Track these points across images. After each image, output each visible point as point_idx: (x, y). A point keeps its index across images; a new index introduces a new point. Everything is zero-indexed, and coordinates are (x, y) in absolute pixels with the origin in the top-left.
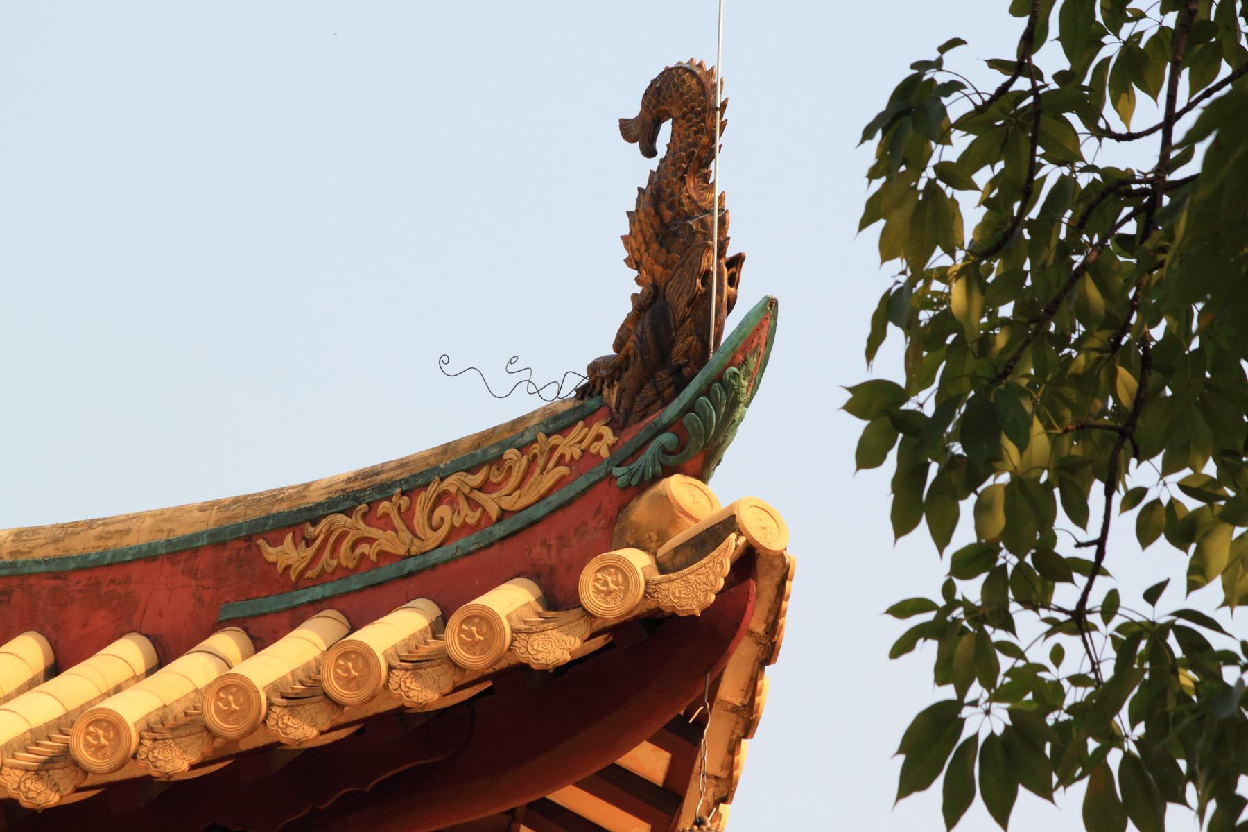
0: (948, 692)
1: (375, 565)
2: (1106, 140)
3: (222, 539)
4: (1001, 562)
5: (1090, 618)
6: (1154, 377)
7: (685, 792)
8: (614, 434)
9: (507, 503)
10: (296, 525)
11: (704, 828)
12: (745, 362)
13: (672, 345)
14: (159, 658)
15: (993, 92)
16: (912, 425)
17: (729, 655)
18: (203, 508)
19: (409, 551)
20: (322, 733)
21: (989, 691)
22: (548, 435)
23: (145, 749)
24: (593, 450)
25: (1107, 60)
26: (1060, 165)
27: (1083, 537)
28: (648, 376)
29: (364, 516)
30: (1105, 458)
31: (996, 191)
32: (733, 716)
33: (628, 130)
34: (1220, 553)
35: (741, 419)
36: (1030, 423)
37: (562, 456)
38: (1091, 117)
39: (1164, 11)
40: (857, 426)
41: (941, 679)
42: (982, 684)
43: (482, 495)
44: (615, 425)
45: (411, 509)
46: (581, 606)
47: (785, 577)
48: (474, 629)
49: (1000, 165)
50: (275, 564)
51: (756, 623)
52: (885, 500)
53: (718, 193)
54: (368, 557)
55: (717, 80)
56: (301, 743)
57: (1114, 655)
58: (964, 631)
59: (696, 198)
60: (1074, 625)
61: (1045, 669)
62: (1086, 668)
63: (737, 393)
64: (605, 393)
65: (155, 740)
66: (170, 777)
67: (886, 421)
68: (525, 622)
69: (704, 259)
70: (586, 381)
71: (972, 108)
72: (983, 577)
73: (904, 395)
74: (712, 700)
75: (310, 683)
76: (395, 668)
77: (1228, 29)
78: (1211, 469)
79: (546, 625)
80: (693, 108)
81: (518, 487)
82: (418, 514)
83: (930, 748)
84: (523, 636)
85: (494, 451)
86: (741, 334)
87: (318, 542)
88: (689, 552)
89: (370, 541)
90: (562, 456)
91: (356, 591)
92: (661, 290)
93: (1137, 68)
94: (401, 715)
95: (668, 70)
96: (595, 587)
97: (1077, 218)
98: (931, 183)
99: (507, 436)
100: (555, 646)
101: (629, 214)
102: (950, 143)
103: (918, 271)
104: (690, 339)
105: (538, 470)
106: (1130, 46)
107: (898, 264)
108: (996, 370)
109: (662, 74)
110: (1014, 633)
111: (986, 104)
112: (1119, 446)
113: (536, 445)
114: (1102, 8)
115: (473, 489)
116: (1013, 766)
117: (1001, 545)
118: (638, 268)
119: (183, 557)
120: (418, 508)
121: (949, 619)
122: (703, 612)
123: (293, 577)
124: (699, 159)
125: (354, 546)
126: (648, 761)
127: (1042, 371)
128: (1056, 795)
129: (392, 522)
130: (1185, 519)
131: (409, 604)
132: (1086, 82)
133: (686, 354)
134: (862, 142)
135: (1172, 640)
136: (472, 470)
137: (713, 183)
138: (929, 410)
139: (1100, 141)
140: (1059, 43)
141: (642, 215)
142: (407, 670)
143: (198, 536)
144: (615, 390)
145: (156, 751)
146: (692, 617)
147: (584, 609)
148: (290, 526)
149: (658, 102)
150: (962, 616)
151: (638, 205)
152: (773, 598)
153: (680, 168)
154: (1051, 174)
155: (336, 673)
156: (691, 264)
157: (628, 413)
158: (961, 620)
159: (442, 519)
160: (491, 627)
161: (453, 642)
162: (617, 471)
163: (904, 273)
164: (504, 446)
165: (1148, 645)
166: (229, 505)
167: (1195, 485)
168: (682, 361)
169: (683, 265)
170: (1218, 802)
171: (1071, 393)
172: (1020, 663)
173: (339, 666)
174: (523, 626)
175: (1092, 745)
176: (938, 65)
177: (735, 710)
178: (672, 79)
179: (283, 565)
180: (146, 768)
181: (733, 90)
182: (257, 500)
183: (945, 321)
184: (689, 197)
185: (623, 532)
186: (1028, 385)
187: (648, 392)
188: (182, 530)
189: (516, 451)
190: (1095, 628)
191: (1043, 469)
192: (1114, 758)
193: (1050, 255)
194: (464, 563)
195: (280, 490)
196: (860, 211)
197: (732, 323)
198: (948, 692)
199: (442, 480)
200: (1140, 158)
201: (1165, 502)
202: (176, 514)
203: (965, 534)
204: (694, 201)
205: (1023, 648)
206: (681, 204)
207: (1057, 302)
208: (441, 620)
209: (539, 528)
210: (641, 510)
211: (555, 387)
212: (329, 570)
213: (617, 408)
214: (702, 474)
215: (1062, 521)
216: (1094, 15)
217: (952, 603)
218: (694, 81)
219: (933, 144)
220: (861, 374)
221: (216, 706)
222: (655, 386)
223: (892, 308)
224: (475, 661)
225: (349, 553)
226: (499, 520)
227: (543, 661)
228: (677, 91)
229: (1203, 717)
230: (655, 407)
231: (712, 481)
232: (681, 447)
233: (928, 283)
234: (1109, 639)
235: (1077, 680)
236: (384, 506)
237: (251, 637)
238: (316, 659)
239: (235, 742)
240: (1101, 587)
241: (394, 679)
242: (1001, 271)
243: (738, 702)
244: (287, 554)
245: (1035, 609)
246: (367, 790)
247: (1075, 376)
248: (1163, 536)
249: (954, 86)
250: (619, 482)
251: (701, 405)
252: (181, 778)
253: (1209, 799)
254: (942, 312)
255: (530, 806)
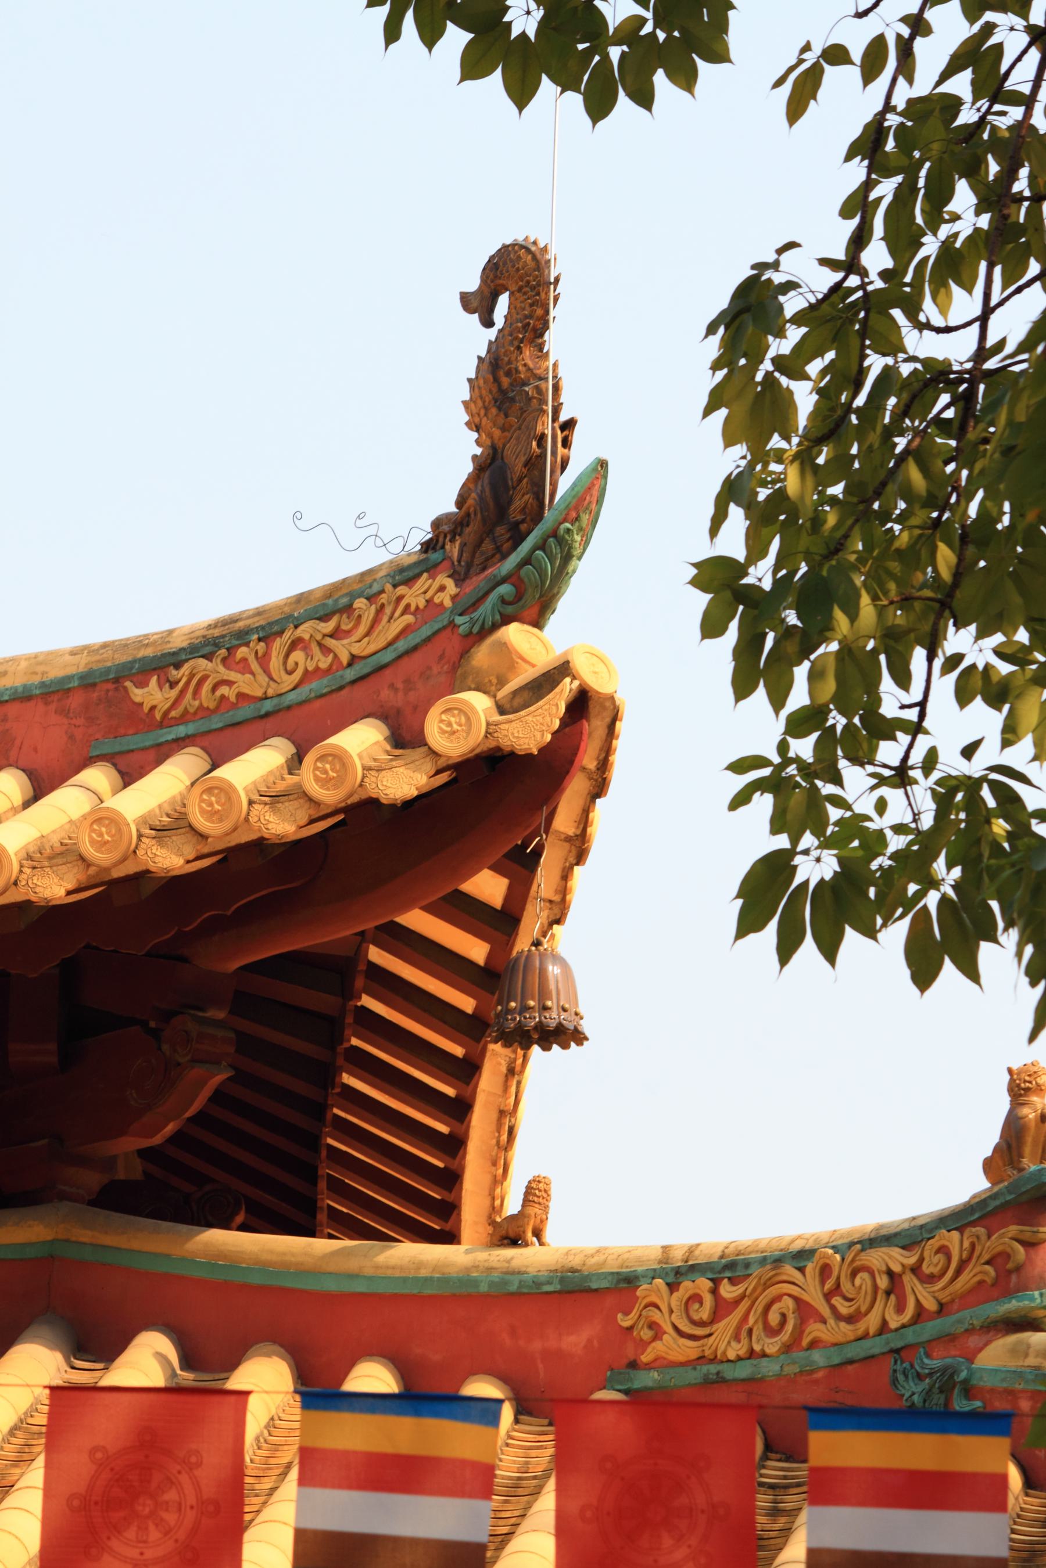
0: (783, 841)
1: (234, 706)
2: (926, 332)
3: (91, 681)
4: (831, 722)
5: (911, 773)
6: (971, 550)
7: (522, 915)
8: (456, 585)
9: (356, 649)
10: (161, 668)
11: (541, 948)
12: (577, 519)
13: (510, 502)
14: (34, 790)
15: (825, 291)
16: (750, 596)
17: (563, 791)
18: (73, 653)
19: (265, 693)
20: (188, 862)
21: (819, 839)
22: (395, 586)
23: (24, 876)
24: (437, 600)
25: (926, 258)
26: (884, 355)
27: (907, 699)
28: (488, 531)
29: (224, 660)
30: (926, 627)
31: (828, 378)
32: (567, 845)
33: (467, 302)
34: (1030, 714)
35: (574, 571)
36: (859, 596)
37: (408, 606)
38: (912, 311)
39: (978, 213)
40: (702, 600)
41: (775, 830)
42: (813, 833)
43: (333, 641)
44: (457, 577)
45: (267, 654)
46: (426, 744)
47: (615, 718)
48: (328, 766)
49: (831, 355)
50: (141, 704)
51: (588, 760)
52: (727, 666)
53: (552, 361)
54: (228, 699)
55: (550, 256)
56: (168, 871)
57: (934, 806)
58: (797, 785)
59: (531, 366)
60: (897, 780)
61: (869, 819)
62: (908, 818)
63: (570, 548)
64: (448, 547)
65: (34, 868)
66: (49, 901)
67: (728, 595)
68: (375, 760)
69: (540, 423)
70: (430, 536)
71: (806, 305)
72: (815, 736)
73: (741, 570)
74: (547, 832)
75: (176, 815)
76: (255, 802)
77: (1036, 230)
78: (1022, 636)
79: (394, 763)
80: (528, 282)
81: (367, 634)
82: (274, 659)
83: (765, 892)
84: (373, 773)
85: (344, 601)
86: (574, 493)
87: (181, 684)
88: (526, 695)
89: (229, 683)
90: (408, 606)
91: (215, 730)
92: (500, 451)
93: (953, 265)
94: (260, 845)
95: (505, 248)
96: (440, 728)
97: (902, 407)
98: (768, 375)
99: (356, 587)
100: (403, 782)
101: (469, 380)
102: (785, 337)
103: (759, 455)
104: (527, 497)
105: (385, 619)
106: (947, 246)
107: (740, 449)
108: (828, 548)
109: (500, 250)
110: (842, 787)
111: (820, 302)
112: (939, 615)
113: (383, 595)
114: (923, 211)
115: (325, 635)
116: (839, 911)
117: (832, 706)
118: (477, 431)
119: (56, 698)
120: (274, 653)
121: (783, 774)
122: (540, 750)
123: (158, 716)
124: (535, 330)
125: (214, 688)
126: (488, 886)
127: (869, 547)
128: (879, 936)
129: (249, 666)
130: (999, 683)
131: (267, 742)
132: (908, 279)
133: (523, 510)
134: (706, 337)
135: (986, 793)
136: (324, 618)
137: (548, 352)
138: (767, 585)
139: (921, 332)
140: (883, 243)
141: (481, 382)
142: (266, 804)
143: (70, 678)
144: (457, 544)
145: (35, 878)
146: (529, 756)
147: (430, 748)
148: (155, 669)
149: (496, 277)
150: (795, 772)
151: (477, 372)
152: (604, 736)
153: (517, 338)
154: (876, 363)
155: (200, 807)
156: (527, 427)
157: (469, 566)
158: (794, 776)
159: (297, 664)
160: (344, 765)
161: (308, 777)
162: (459, 620)
163: (744, 457)
164: (353, 596)
165: (964, 796)
166: (98, 650)
167: (1008, 651)
168: (519, 517)
169: (520, 428)
170: (1035, 947)
171: (895, 566)
172: (848, 814)
173: (202, 801)
174: (373, 764)
175: (912, 888)
176: (775, 266)
177: (568, 839)
178: (509, 255)
179: (149, 706)
180: (26, 894)
181: (563, 265)
182: (124, 645)
183: (779, 497)
184: (525, 365)
185: (464, 676)
186: (857, 559)
187: (488, 546)
188: (55, 673)
189: (365, 601)
190: (916, 782)
191: (870, 637)
192: (932, 900)
193: (874, 438)
194: (318, 704)
195: (145, 636)
196: (704, 400)
197: (565, 482)
198: (783, 841)
199: (296, 627)
200: (957, 350)
201: (981, 666)
202: (51, 656)
203: (799, 697)
204: (529, 369)
205: (850, 801)
206: (517, 371)
207: (884, 484)
208: (296, 758)
209: (388, 672)
210: (482, 656)
211: (400, 543)
212: (192, 710)
213: (459, 561)
214: (538, 623)
215: (887, 683)
216: (914, 217)
217: (787, 761)
218: (530, 257)
219: (770, 338)
220: (705, 551)
221: (90, 837)
222: (494, 540)
223: (733, 490)
224: (330, 796)
225: (210, 695)
226: (350, 665)
227: (392, 796)
228: (513, 266)
229: (1021, 870)
230: (495, 560)
231: (547, 629)
232: (519, 596)
233: (766, 465)
234: (929, 792)
235: (899, 829)
236: (242, 652)
237: (119, 772)
238: (181, 794)
239: (107, 870)
240: (922, 744)
241: (254, 813)
242: (831, 455)
243: (571, 831)
244: (152, 695)
245: (862, 765)
246: (229, 913)
247: (898, 551)
248: (979, 698)
249: (790, 286)
250: (461, 630)
251: (538, 559)
252: (58, 903)
253: (1027, 943)
254: (775, 491)
255: (378, 928)
